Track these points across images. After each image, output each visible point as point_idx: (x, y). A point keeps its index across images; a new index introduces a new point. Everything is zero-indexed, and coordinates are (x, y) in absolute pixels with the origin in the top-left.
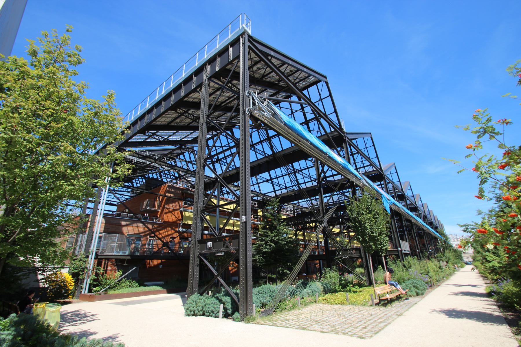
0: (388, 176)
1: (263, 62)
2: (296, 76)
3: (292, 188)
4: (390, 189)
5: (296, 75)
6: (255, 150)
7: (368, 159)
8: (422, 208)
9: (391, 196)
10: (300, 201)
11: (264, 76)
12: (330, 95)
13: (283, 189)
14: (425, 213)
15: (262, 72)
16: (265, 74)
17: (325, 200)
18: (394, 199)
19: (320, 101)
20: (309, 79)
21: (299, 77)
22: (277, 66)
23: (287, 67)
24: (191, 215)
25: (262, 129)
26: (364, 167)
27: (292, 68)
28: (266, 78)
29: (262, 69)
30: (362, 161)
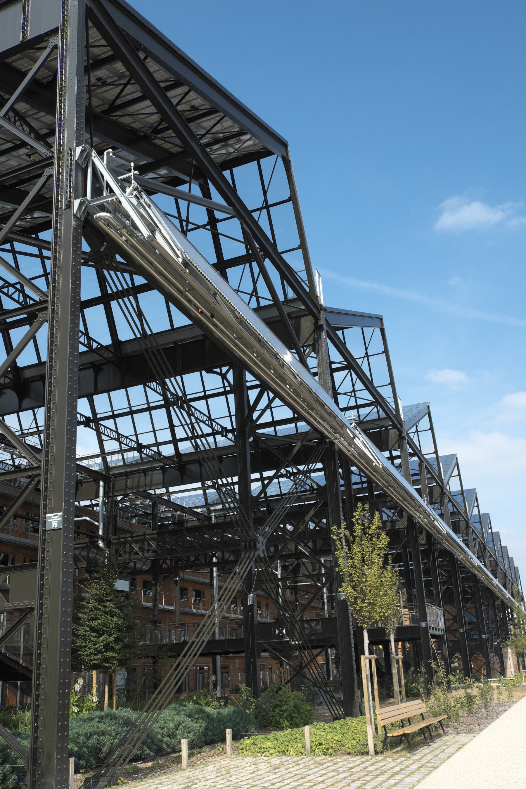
1: (396, 430)
2: (205, 124)
3: (155, 449)
5: (207, 122)
6: (212, 424)
7: (369, 385)
10: (171, 489)
11: (113, 107)
12: (432, 429)
13: (132, 449)
14: (483, 537)
15: (111, 93)
16: (119, 102)
17: (256, 487)
19: (264, 211)
20: (239, 141)
21: (213, 130)
22: (162, 85)
23: (187, 94)
25: (116, 270)
26: (357, 407)
27: (198, 102)
28: (119, 113)
29: (110, 84)
30: (354, 391)
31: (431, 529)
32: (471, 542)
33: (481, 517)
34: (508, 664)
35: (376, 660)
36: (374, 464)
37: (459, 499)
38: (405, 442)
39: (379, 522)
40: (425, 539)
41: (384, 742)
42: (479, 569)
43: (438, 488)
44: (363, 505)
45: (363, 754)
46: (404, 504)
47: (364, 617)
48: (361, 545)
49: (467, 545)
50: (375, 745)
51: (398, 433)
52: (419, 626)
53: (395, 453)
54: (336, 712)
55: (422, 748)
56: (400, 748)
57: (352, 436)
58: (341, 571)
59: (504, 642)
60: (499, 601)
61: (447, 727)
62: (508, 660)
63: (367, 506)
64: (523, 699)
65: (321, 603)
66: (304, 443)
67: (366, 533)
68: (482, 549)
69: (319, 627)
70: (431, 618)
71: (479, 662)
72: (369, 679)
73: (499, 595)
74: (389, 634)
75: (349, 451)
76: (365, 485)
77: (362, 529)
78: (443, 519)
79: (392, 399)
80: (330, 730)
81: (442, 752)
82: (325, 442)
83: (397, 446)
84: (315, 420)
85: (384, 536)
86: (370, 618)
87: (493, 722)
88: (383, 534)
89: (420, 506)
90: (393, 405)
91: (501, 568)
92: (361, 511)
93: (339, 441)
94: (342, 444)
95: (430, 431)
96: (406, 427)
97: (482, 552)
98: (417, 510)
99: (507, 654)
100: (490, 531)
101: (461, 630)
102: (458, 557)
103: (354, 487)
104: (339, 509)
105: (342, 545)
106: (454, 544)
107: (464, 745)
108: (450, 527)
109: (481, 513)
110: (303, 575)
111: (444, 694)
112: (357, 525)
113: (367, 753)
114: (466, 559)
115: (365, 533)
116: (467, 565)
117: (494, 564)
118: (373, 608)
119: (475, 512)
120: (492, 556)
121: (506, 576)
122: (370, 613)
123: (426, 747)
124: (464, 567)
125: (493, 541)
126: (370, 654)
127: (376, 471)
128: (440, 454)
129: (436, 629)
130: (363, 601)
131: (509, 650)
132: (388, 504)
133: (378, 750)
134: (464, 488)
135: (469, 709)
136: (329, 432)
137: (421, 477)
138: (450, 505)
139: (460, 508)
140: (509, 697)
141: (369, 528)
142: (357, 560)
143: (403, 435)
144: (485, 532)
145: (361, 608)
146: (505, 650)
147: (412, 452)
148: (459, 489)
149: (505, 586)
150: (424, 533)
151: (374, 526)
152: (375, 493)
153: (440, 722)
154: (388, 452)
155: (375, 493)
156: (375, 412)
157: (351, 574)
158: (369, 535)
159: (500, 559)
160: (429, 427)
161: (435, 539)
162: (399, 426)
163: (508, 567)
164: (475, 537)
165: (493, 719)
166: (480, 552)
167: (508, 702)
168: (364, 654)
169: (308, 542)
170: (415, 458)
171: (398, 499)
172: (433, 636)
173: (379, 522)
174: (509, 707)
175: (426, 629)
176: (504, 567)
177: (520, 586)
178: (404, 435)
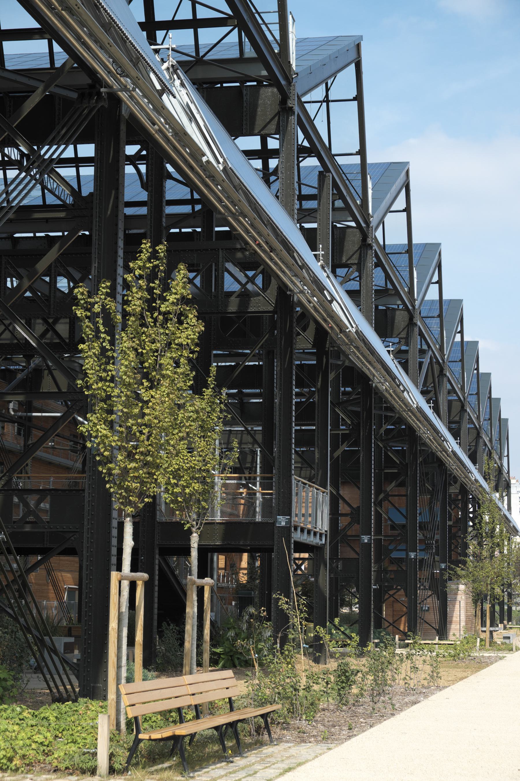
0: (311, 109)
1: (275, 90)
4: (306, 191)
8: (457, 368)
9: (302, 229)
12: (359, 98)
18: (313, 247)
19: (325, 104)
24: (48, 506)
31: (325, 321)
32: (413, 359)
33: (444, 307)
34: (456, 613)
35: (148, 585)
36: (204, 159)
37: (402, 261)
38: (293, 119)
39: (184, 288)
40: (311, 339)
41: (133, 750)
42: (418, 415)
43: (357, 232)
44: (153, 246)
45: (83, 772)
46: (271, 259)
47: (128, 490)
48: (138, 335)
49: (405, 366)
50: (111, 756)
51: (279, 96)
52: (274, 524)
53: (273, 144)
54: (69, 687)
55: (213, 767)
56: (166, 765)
57: (158, 87)
58: (89, 388)
59: (452, 569)
60: (458, 485)
61: (284, 729)
62: (457, 606)
63: (161, 248)
64: (461, 683)
65: (81, 460)
66: (52, 89)
67: (155, 309)
68: (436, 374)
69: (45, 505)
70: (307, 510)
71: (397, 606)
72: (126, 621)
73: (458, 473)
74: (189, 532)
75: (154, 124)
76: (198, 207)
77: (147, 301)
78: (358, 304)
79: (275, 18)
80: (34, 723)
81: (250, 775)
82: (99, 94)
83: (273, 127)
84: (79, 38)
85: (194, 320)
86: (141, 495)
87: (380, 722)
88: (190, 316)
89: (305, 266)
90: (276, 29)
91: (470, 418)
92: (149, 260)
93: (132, 97)
94: (138, 103)
95: (355, 103)
96: (298, 87)
97: (434, 382)
98: (296, 275)
99: (456, 594)
100: (458, 338)
101: (365, 539)
102: (379, 385)
103: (170, 210)
104: (116, 252)
105: (97, 331)
106: (371, 357)
107: (300, 764)
108: (368, 318)
109: (445, 297)
110: (49, 395)
111: (288, 663)
112: (134, 290)
113: (93, 771)
114: (394, 392)
115: (152, 310)
116: (397, 405)
117: (456, 407)
118: (151, 474)
119: (433, 294)
120: (456, 392)
121: (478, 436)
122: (142, 483)
123: (224, 764)
124: (391, 409)
125: (462, 360)
126: (132, 570)
127: (212, 177)
128: (370, 160)
129: (309, 532)
130: (130, 456)
131: (462, 587)
132: (239, 255)
133: (117, 766)
134: (415, 241)
135: (340, 695)
136: (109, 72)
137: (319, 204)
138: (378, 274)
139: (400, 283)
140: (432, 677)
141: (164, 299)
142: (126, 366)
143: (290, 103)
144: (448, 338)
145: (125, 471)
146: (454, 587)
147: (306, 144)
148: (405, 241)
149: (473, 458)
150: (312, 327)
151: (174, 296)
152: (217, 229)
153: (264, 716)
154: (258, 138)
155: (217, 229)
156: (230, 46)
157: (109, 397)
158: (160, 313)
159: (473, 400)
160: (354, 93)
161: (333, 342)
162: (283, 82)
163: (487, 417)
164: (425, 347)
165: (383, 717)
166: (430, 379)
167: (428, 687)
168: (119, 568)
169: (56, 321)
170: (312, 162)
171: (259, 245)
172: (301, 547)
173: (184, 288)
174: (426, 696)
175: (287, 531)
176: (478, 418)
177: (505, 460)
178: (293, 103)
